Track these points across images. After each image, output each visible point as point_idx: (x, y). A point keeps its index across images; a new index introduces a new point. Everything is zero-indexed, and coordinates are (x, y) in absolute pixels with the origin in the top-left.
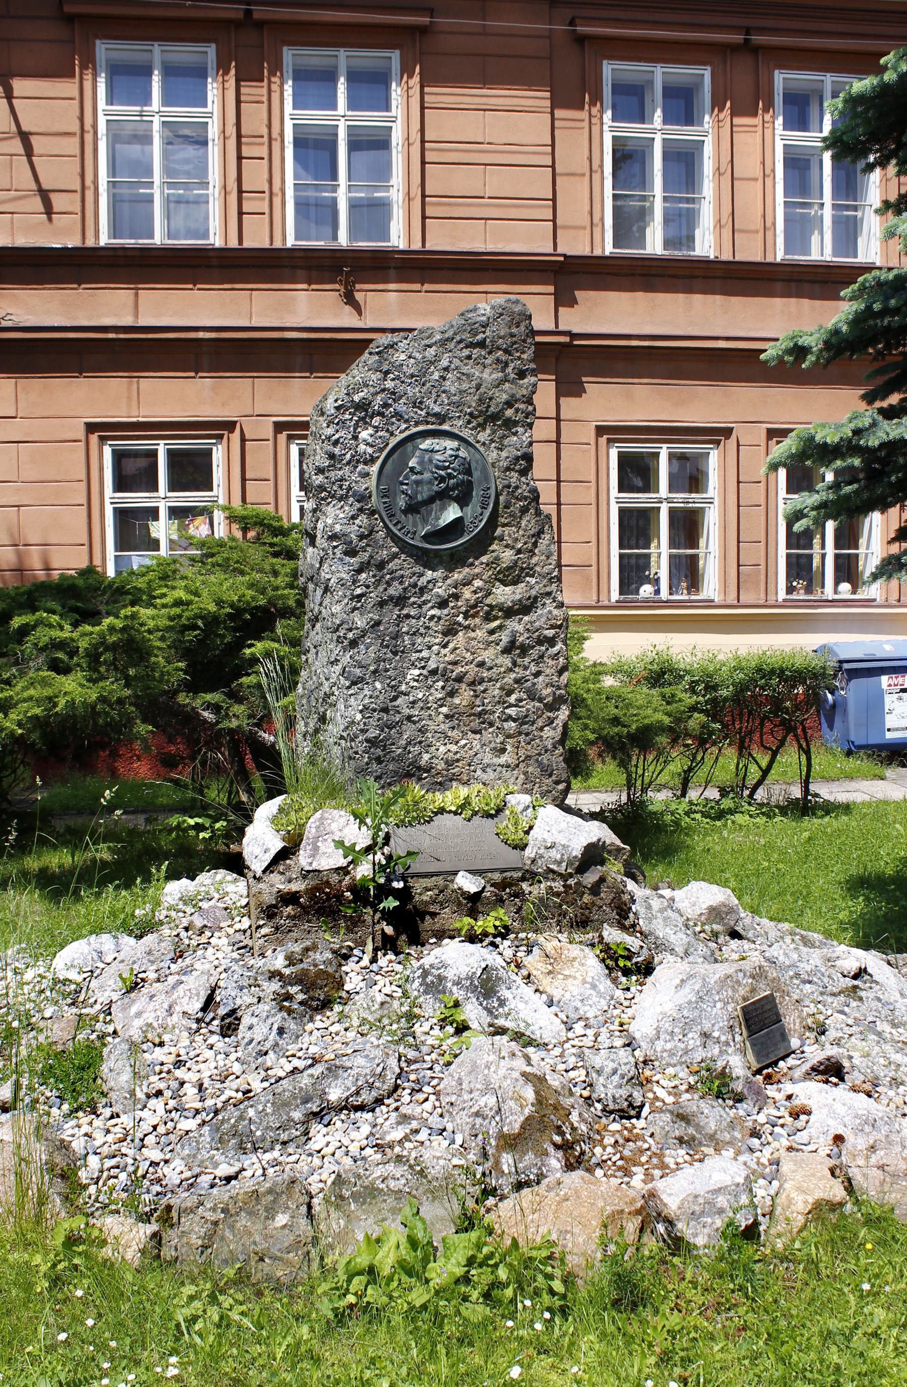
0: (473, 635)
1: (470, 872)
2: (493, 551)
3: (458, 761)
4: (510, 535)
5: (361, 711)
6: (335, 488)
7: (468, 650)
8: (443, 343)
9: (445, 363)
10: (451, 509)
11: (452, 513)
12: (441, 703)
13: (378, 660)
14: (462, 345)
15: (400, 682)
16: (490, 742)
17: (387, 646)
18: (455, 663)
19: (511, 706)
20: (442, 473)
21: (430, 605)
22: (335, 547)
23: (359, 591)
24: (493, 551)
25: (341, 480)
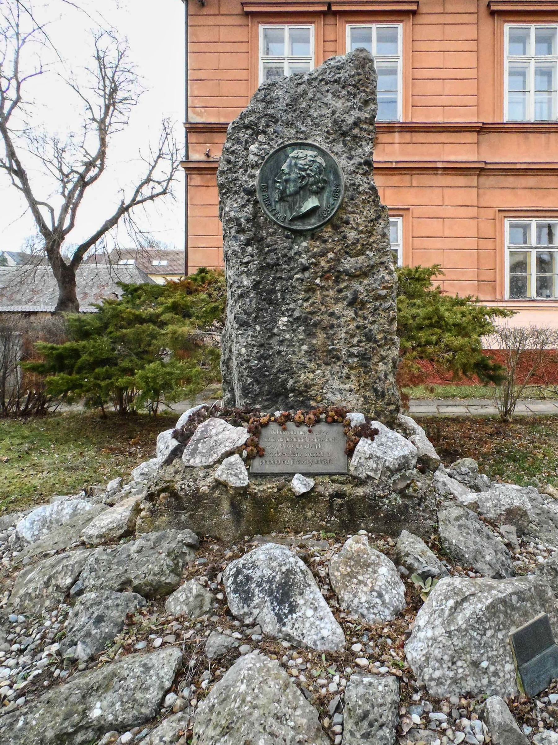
0: (327, 293)
1: (304, 474)
2: (342, 232)
3: (314, 385)
4: (354, 220)
5: (245, 347)
6: (231, 186)
7: (323, 304)
8: (310, 82)
9: (311, 95)
10: (310, 200)
11: (311, 203)
12: (302, 342)
13: (258, 310)
14: (323, 83)
15: (273, 326)
16: (338, 372)
17: (264, 300)
18: (312, 313)
19: (353, 346)
20: (303, 173)
21: (296, 270)
22: (230, 228)
23: (246, 260)
24: (342, 232)
25: (235, 180)
